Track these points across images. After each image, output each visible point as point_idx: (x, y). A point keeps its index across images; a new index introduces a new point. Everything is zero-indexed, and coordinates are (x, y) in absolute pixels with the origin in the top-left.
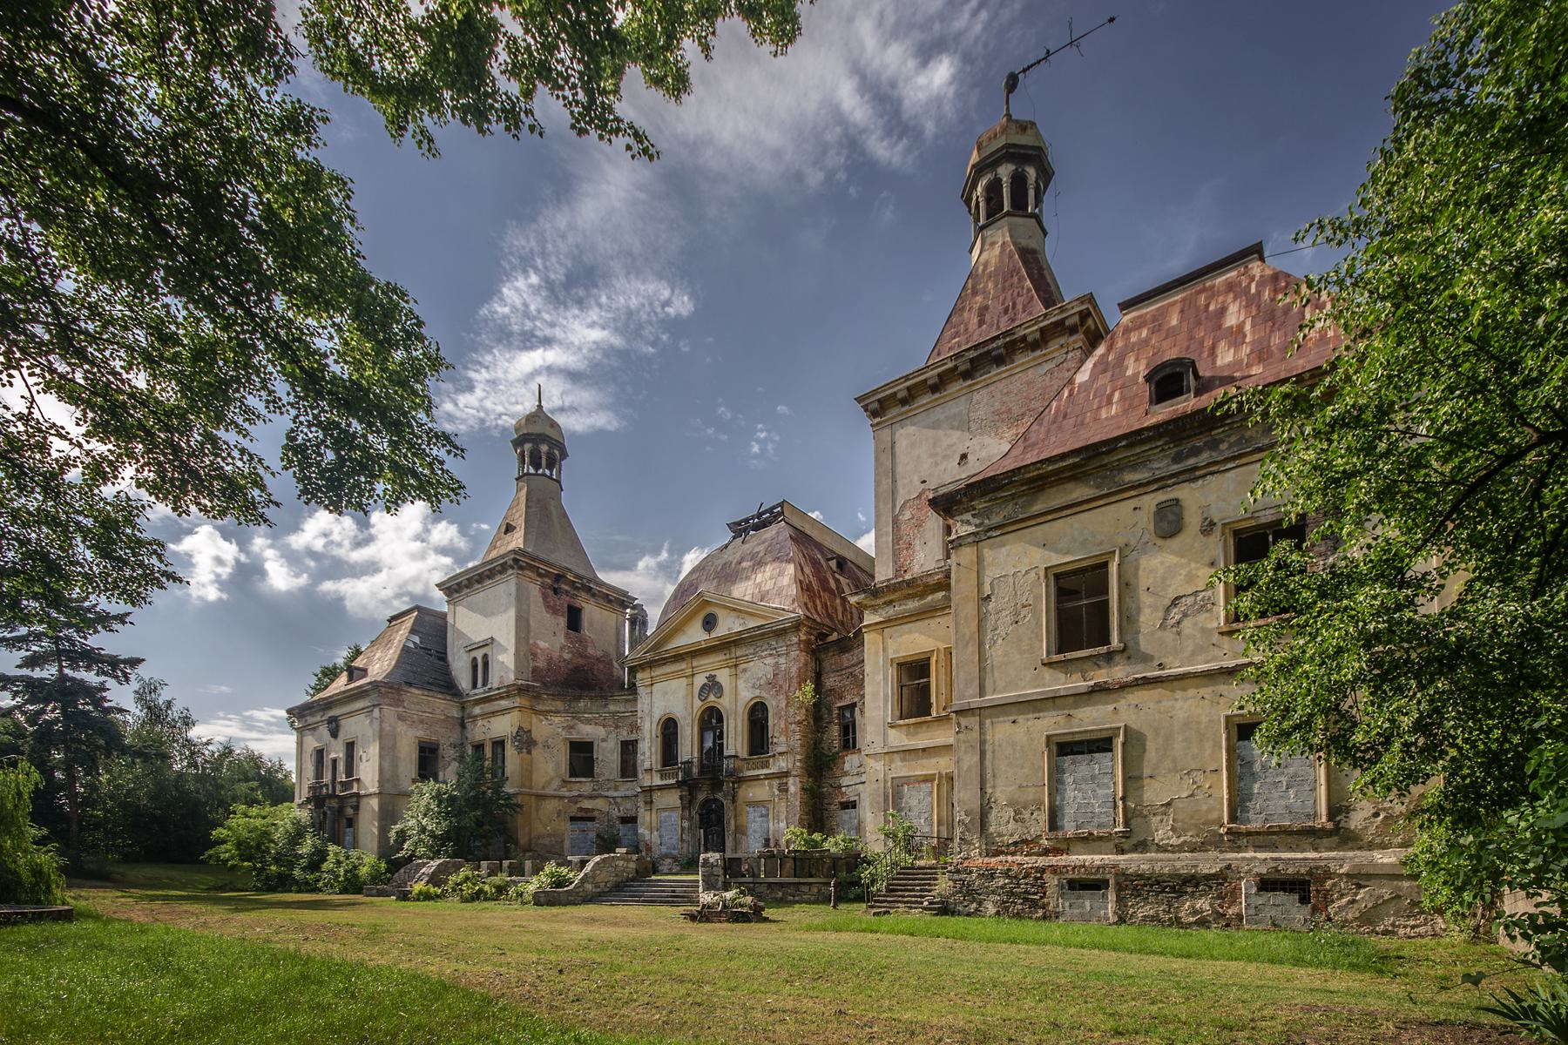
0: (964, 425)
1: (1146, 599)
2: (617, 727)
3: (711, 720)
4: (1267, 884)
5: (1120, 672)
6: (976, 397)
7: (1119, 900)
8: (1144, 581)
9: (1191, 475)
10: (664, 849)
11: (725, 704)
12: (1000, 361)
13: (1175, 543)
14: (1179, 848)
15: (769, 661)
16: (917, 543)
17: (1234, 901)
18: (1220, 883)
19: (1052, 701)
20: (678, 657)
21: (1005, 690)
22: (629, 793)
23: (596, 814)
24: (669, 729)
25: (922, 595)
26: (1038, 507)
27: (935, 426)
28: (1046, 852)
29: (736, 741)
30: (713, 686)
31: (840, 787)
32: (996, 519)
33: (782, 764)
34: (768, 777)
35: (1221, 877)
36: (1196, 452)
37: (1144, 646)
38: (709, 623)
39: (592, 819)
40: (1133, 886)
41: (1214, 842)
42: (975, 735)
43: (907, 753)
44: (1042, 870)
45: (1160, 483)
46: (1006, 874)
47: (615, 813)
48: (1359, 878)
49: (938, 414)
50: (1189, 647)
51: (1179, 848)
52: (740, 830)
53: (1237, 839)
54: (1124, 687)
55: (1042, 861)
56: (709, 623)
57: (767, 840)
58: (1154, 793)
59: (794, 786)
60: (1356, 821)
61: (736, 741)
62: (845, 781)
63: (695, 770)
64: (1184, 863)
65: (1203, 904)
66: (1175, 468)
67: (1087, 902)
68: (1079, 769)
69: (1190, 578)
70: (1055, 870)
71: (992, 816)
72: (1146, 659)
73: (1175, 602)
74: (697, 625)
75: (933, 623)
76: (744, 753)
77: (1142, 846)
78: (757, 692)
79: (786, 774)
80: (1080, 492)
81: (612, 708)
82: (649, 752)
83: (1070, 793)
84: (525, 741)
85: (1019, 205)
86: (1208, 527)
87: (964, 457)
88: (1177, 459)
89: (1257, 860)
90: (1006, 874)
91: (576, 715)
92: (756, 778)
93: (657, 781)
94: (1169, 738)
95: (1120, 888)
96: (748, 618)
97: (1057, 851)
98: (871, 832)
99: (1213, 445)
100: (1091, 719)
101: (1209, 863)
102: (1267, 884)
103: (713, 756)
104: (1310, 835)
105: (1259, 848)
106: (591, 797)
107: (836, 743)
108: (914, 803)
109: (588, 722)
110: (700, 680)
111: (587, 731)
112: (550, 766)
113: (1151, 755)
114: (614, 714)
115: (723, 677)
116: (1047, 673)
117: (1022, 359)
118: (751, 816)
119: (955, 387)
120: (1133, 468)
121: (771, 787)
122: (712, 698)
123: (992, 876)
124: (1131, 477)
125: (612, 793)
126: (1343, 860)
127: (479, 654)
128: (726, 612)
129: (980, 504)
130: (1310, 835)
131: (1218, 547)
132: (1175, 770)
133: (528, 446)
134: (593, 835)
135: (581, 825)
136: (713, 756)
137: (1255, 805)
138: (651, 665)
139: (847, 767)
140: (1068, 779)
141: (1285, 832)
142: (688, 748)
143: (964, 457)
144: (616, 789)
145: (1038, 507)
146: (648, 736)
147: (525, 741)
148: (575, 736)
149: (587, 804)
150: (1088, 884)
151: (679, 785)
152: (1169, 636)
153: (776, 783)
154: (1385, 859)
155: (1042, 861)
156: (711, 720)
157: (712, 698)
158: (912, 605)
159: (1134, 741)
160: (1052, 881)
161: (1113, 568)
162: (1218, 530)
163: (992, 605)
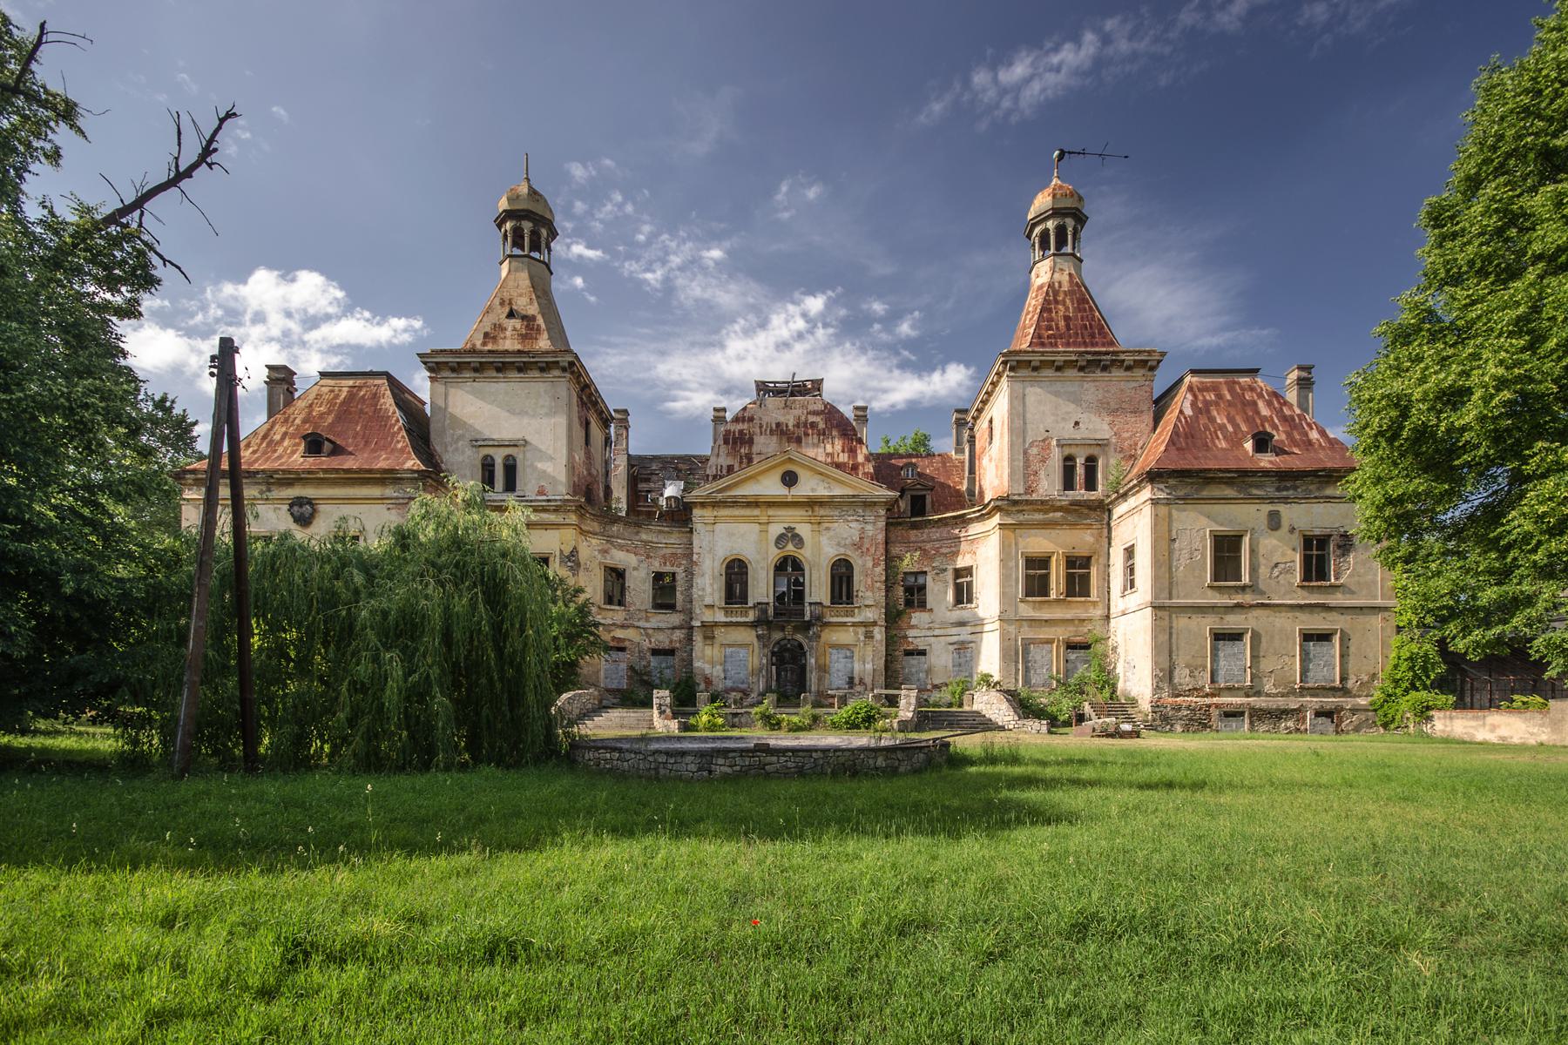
0: (1077, 401)
1: (1262, 560)
2: (648, 557)
3: (789, 568)
4: (1318, 714)
5: (1248, 598)
6: (1086, 385)
7: (1251, 723)
8: (1262, 550)
9: (1285, 500)
10: (729, 683)
11: (805, 554)
12: (1105, 368)
13: (1277, 533)
14: (1276, 695)
15: (854, 525)
16: (1042, 474)
17: (1304, 722)
18: (1298, 713)
19: (1213, 609)
20: (754, 503)
21: (1185, 597)
22: (662, 625)
23: (627, 644)
24: (736, 573)
25: (1046, 512)
26: (1205, 493)
27: (1057, 394)
28: (1207, 695)
29: (818, 589)
30: (790, 536)
31: (906, 637)
32: (1181, 493)
33: (870, 615)
34: (854, 625)
35: (1298, 711)
36: (1287, 489)
37: (1261, 586)
38: (790, 479)
39: (622, 649)
40: (1258, 715)
41: (1292, 692)
42: (1167, 622)
43: (1033, 622)
44: (1209, 706)
45: (1272, 500)
46: (1188, 708)
47: (646, 644)
48: (1354, 711)
49: (1058, 386)
50: (1283, 590)
51: (1276, 695)
52: (823, 669)
53: (1304, 691)
54: (1251, 606)
55: (1208, 701)
56: (790, 479)
57: (851, 679)
58: (1266, 665)
59: (879, 634)
60: (1350, 684)
61: (818, 589)
62: (911, 633)
63: (771, 611)
64: (1281, 703)
65: (1290, 724)
66: (1277, 494)
67: (1233, 722)
68: (1226, 648)
69: (1284, 555)
70: (1217, 706)
71: (1176, 673)
72: (1262, 593)
73: (1276, 565)
74: (775, 477)
75: (1054, 533)
76: (827, 602)
77: (1258, 694)
78: (842, 550)
79: (874, 624)
80: (1229, 492)
81: (644, 537)
82: (708, 587)
83: (1222, 663)
84: (572, 559)
85: (1061, 242)
86: (1292, 530)
87: (1077, 423)
88: (1278, 489)
89: (1314, 702)
90: (1188, 708)
91: (610, 539)
92: (844, 624)
93: (721, 617)
94: (1272, 637)
95: (1251, 716)
96: (833, 483)
97: (1213, 695)
98: (1350, 684)
99: (1295, 488)
100: (1233, 622)
101: (1293, 703)
102: (1318, 714)
103: (791, 599)
104: (1333, 690)
105: (1312, 696)
106: (623, 627)
107: (902, 601)
108: (1038, 658)
109: (621, 548)
110: (776, 529)
111: (620, 558)
112: (592, 586)
113: (1264, 645)
114: (646, 543)
115: (804, 530)
116: (1210, 592)
117: (1117, 373)
118: (834, 657)
119: (1071, 373)
120: (1257, 487)
121: (856, 633)
122: (790, 547)
123: (1180, 709)
124: (1255, 492)
125: (641, 624)
126: (1348, 703)
127: (499, 456)
128: (808, 473)
129: (1172, 482)
130: (1333, 690)
131: (1297, 541)
132: (1275, 654)
133: (508, 225)
134: (623, 666)
135: (615, 655)
136: (791, 599)
137: (1310, 674)
138: (716, 504)
139: (914, 622)
140: (1221, 654)
141: (1324, 688)
142: (762, 588)
143: (1077, 423)
144: (647, 620)
145: (1205, 493)
146: (709, 573)
147: (572, 559)
148: (609, 562)
149: (619, 633)
150: (1232, 714)
151: (753, 625)
152: (1273, 583)
153: (861, 630)
154: (1363, 701)
155: (1208, 701)
156: (789, 568)
157: (790, 547)
158: (1039, 517)
159: (1256, 637)
160: (1215, 713)
161: (1246, 540)
162: (1297, 533)
163: (1177, 545)
